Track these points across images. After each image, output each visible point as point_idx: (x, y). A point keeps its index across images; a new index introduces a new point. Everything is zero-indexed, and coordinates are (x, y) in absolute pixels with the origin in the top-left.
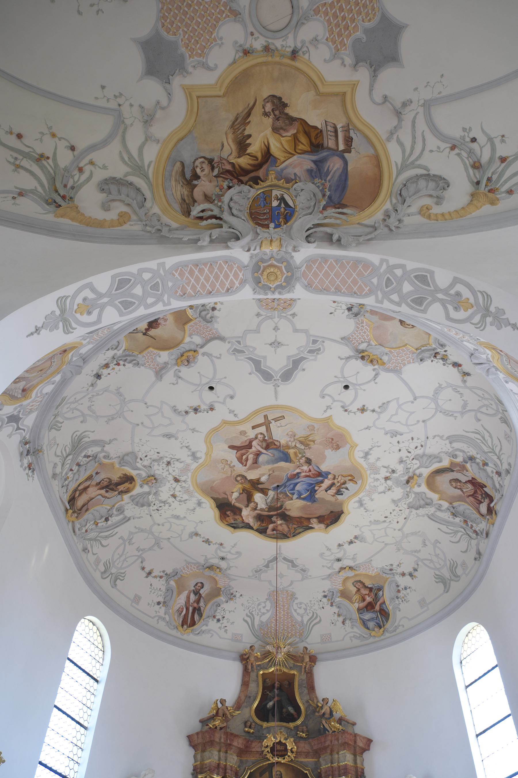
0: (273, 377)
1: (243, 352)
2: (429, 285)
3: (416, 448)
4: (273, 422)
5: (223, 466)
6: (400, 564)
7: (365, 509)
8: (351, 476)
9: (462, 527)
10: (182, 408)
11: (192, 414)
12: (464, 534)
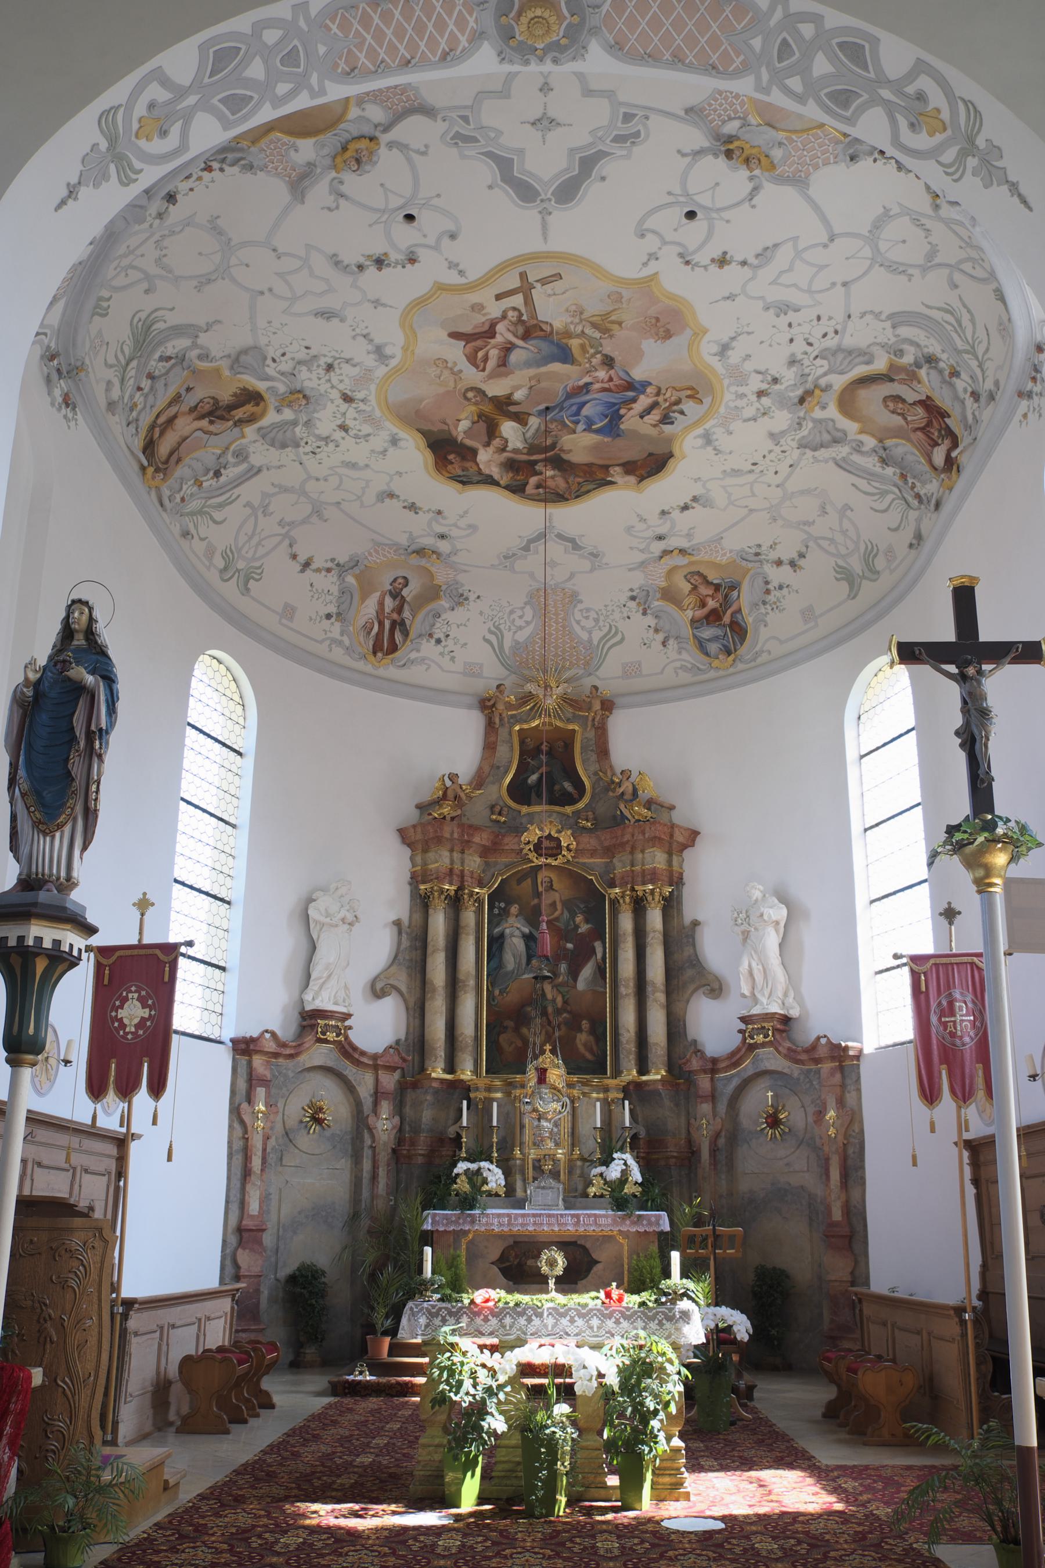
0: (538, 194)
1: (475, 140)
2: (866, 68)
3: (825, 335)
4: (538, 285)
5: (438, 372)
6: (775, 544)
7: (715, 449)
8: (692, 388)
9: (895, 485)
10: (351, 258)
11: (372, 270)
12: (898, 498)
